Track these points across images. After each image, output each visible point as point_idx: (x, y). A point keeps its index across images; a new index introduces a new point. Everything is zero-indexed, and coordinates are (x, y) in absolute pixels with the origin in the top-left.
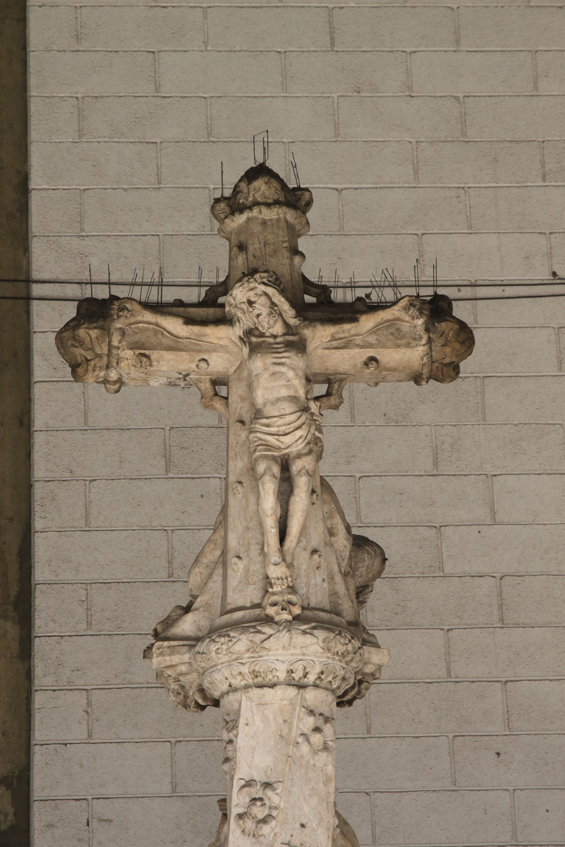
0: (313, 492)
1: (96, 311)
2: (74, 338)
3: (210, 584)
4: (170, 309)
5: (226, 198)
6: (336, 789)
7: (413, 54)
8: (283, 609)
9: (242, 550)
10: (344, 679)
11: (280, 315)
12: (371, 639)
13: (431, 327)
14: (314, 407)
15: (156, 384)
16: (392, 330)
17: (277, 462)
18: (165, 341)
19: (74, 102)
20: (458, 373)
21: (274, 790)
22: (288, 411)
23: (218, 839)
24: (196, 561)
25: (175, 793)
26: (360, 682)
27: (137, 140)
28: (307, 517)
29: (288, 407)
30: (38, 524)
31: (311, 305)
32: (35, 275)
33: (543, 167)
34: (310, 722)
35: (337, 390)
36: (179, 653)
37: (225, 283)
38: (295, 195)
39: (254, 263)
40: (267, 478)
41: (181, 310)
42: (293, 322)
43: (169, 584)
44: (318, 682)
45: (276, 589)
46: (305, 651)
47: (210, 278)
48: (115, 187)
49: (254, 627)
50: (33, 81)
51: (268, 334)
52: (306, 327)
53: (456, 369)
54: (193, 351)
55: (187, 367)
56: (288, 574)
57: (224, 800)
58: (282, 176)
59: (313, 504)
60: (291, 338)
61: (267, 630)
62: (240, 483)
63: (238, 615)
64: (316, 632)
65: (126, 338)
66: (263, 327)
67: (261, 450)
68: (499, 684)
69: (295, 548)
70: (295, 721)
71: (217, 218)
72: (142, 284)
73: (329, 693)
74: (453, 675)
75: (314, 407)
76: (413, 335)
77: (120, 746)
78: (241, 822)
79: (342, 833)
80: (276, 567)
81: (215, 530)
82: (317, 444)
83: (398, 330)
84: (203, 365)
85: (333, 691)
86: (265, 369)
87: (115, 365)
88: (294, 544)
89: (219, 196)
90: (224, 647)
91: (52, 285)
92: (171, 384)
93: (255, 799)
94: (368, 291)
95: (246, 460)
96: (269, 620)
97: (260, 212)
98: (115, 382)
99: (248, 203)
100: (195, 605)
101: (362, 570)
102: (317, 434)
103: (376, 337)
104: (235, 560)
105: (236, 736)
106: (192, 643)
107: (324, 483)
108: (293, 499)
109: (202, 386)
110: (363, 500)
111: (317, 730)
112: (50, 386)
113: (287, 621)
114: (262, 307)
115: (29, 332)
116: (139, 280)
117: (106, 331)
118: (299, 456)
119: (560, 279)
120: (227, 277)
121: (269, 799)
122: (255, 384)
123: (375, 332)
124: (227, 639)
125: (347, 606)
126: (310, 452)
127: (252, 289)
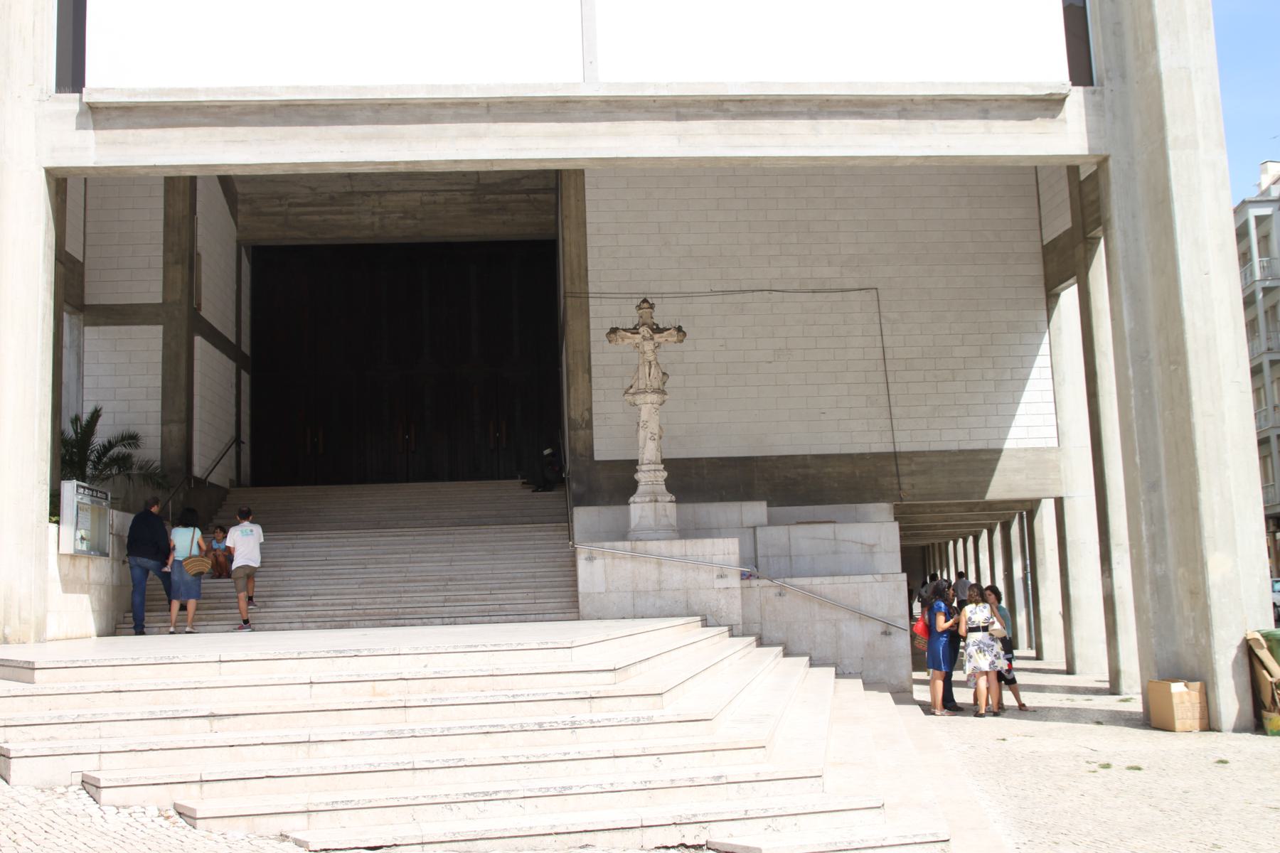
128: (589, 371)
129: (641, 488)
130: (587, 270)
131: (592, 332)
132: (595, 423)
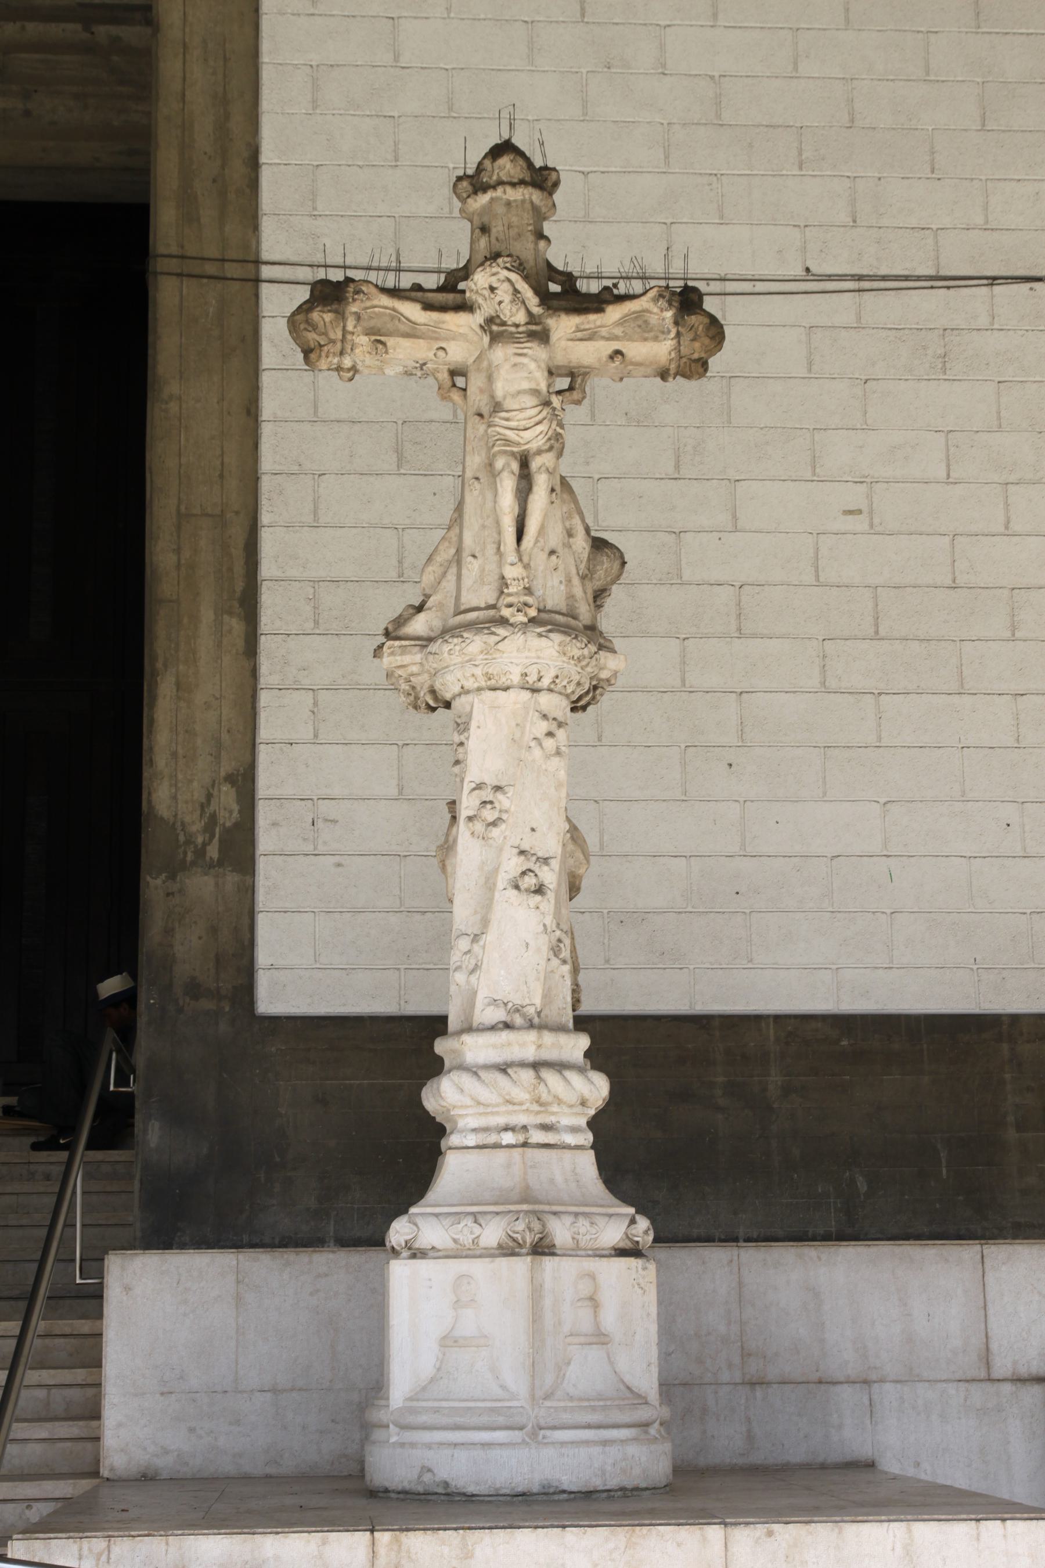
0: (553, 490)
1: (330, 294)
2: (307, 321)
3: (444, 584)
4: (408, 294)
5: (469, 177)
6: (568, 795)
7: (667, 29)
8: (518, 611)
9: (478, 549)
10: (579, 684)
11: (523, 302)
12: (607, 644)
13: (680, 320)
14: (556, 401)
15: (392, 373)
16: (640, 322)
17: (516, 458)
18: (402, 328)
19: (308, 70)
20: (706, 370)
21: (505, 793)
22: (529, 405)
23: (446, 841)
24: (430, 559)
25: (401, 796)
26: (595, 688)
27: (374, 113)
28: (545, 516)
29: (529, 401)
30: (265, 518)
31: (556, 294)
32: (265, 256)
33: (800, 154)
34: (544, 726)
35: (580, 385)
36: (410, 653)
37: (466, 267)
38: (541, 175)
39: (497, 247)
40: (505, 474)
41: (419, 294)
42: (537, 310)
43: (400, 584)
44: (552, 686)
45: (512, 589)
46: (546, 655)
47: (451, 263)
48: (350, 163)
49: (488, 628)
50: (265, 46)
51: (509, 323)
52: (550, 316)
53: (704, 365)
54: (431, 338)
55: (424, 356)
56: (525, 575)
57: (454, 802)
58: (528, 154)
59: (552, 503)
60: (534, 328)
61: (502, 631)
62: (477, 479)
63: (473, 615)
64: (551, 635)
65: (361, 322)
66: (505, 315)
67: (500, 445)
68: (734, 695)
69: (532, 549)
70: (528, 725)
71: (458, 197)
72: (378, 269)
73: (563, 698)
74: (687, 685)
75: (556, 401)
76: (661, 328)
77: (346, 747)
78: (471, 824)
79: (572, 838)
80: (512, 568)
81: (449, 529)
82: (558, 440)
83: (646, 322)
84: (441, 353)
85: (567, 696)
86: (506, 360)
87: (349, 351)
88: (531, 544)
89: (461, 173)
90: (457, 648)
91: (282, 267)
92: (408, 374)
93: (485, 802)
94: (615, 281)
95: (484, 455)
96: (503, 622)
97: (505, 192)
98: (349, 370)
99: (492, 182)
100: (428, 605)
101: (600, 573)
102: (559, 430)
103: (622, 329)
104: (470, 559)
105: (467, 739)
106: (424, 643)
107: (564, 481)
108: (531, 498)
109: (440, 376)
110: (600, 502)
111: (550, 734)
112: (279, 374)
113: (522, 623)
114: (504, 293)
115: (257, 316)
116: (375, 264)
117: (341, 315)
118: (539, 452)
119: (813, 275)
120: (468, 261)
121: (500, 802)
122: (495, 375)
123: (622, 324)
124: (460, 640)
125: (584, 610)
126: (551, 448)
127: (494, 275)
128: (248, 604)
129: (456, 1170)
130: (253, 162)
131: (267, 432)
132: (266, 841)
